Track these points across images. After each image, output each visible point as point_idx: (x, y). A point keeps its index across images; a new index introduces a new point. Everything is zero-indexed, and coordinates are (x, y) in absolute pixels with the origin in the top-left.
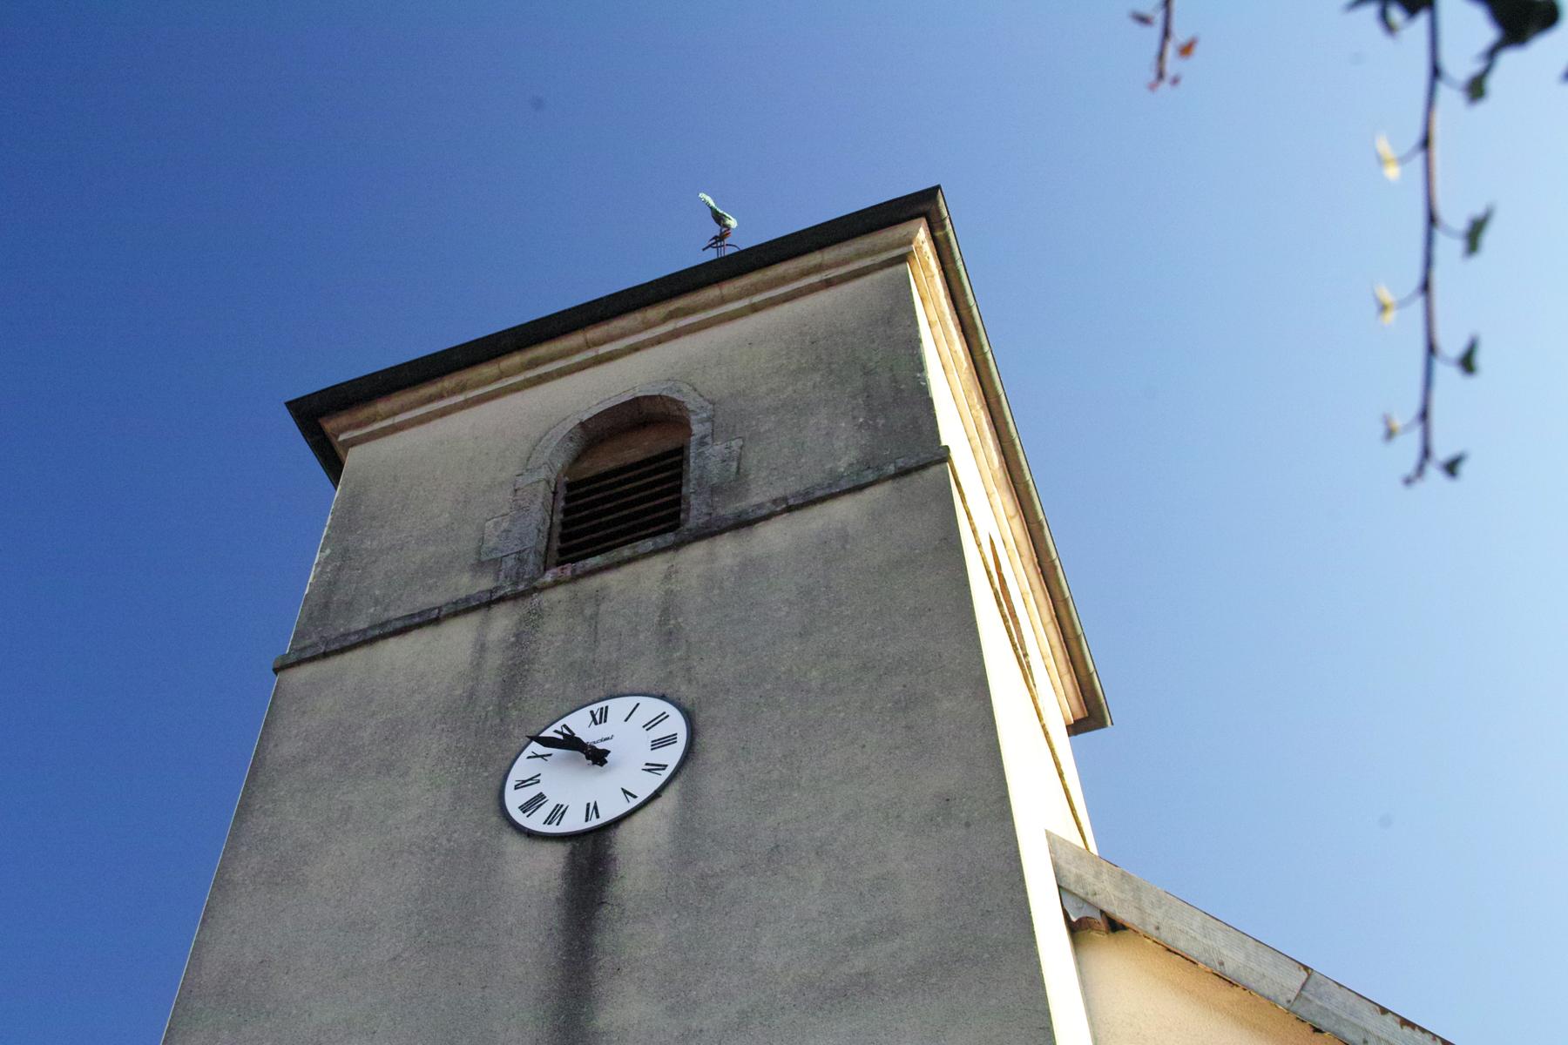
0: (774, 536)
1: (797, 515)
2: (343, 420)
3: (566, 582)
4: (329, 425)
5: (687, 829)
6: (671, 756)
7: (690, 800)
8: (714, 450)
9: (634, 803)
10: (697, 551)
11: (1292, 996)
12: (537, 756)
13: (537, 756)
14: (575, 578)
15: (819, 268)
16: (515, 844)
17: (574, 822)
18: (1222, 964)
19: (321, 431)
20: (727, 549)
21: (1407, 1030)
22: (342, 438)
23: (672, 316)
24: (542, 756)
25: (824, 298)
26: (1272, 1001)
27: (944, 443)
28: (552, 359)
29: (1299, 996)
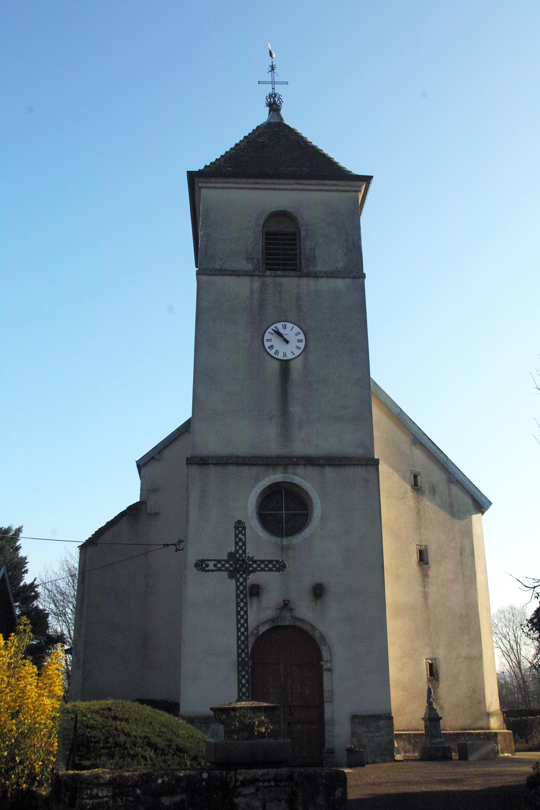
0: (324, 284)
1: (329, 278)
2: (202, 180)
3: (272, 276)
4: (197, 180)
5: (306, 366)
6: (302, 345)
7: (306, 359)
8: (517, 614)
9: (294, 356)
10: (304, 280)
11: (397, 414)
12: (270, 333)
13: (270, 333)
14: (274, 276)
15: (337, 185)
16: (268, 358)
17: (280, 356)
18: (387, 405)
19: (194, 181)
20: (312, 282)
21: (414, 424)
22: (200, 185)
23: (298, 184)
24: (272, 334)
25: (337, 194)
26: (394, 414)
27: (364, 272)
28: (262, 184)
29: (399, 414)
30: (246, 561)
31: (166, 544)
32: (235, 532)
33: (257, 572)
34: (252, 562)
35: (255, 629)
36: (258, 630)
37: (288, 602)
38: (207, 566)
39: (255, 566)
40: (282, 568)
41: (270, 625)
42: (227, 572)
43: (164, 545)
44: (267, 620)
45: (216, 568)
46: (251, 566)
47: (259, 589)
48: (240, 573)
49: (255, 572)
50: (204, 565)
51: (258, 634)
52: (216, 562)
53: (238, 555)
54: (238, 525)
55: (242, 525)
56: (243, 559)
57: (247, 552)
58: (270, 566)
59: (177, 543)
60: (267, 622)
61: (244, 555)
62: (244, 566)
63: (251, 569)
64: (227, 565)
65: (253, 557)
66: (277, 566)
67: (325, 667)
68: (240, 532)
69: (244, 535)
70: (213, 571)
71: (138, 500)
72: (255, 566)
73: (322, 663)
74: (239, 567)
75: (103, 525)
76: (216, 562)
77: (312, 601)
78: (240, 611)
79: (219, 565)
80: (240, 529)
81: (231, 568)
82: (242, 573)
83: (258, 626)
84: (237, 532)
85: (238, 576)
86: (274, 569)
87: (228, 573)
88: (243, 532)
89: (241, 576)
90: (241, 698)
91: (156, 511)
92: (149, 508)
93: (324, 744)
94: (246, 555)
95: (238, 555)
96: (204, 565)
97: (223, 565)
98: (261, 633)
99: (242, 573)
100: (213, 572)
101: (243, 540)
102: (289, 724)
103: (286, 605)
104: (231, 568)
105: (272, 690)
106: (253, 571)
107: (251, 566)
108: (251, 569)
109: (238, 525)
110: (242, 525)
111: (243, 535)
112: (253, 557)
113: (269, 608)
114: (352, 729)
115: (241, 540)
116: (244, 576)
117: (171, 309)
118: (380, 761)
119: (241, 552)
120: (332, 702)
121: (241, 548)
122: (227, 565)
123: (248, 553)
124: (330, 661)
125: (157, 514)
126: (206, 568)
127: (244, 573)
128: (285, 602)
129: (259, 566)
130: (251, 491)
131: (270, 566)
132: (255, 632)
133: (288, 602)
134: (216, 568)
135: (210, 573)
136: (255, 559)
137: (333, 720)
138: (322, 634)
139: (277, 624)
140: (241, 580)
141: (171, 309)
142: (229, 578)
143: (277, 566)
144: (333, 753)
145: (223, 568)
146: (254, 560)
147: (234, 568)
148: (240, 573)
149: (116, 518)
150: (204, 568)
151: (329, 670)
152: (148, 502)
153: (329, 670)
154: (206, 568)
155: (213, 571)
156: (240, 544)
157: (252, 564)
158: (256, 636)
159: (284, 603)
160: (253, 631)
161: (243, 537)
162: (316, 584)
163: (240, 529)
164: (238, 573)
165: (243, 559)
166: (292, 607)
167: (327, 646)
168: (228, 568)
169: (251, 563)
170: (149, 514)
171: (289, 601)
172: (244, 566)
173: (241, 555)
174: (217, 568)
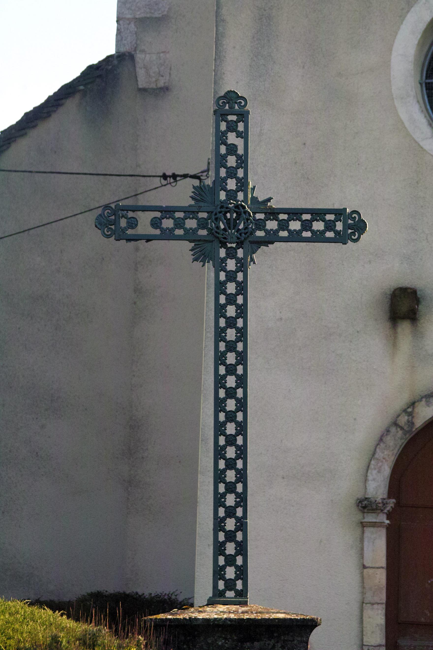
30: (246, 212)
31: (169, 173)
32: (218, 126)
33: (277, 244)
34: (265, 213)
35: (405, 411)
36: (410, 414)
38: (133, 223)
39: (272, 225)
40: (353, 234)
42: (191, 241)
43: (165, 177)
45: (158, 232)
46: (260, 225)
48: (229, 245)
49: (272, 243)
50: (123, 223)
51: (411, 423)
52: (158, 214)
53: (223, 196)
54: (227, 107)
55: (236, 107)
56: (237, 207)
57: (251, 186)
58: (318, 226)
59: (202, 172)
61: (240, 196)
62: (241, 226)
63: (260, 234)
64: (191, 224)
65: (269, 200)
66: (339, 226)
68: (232, 127)
69: (244, 135)
70: (149, 239)
71: (112, 51)
72: (272, 225)
74: (225, 230)
75: (13, 122)
76: (158, 214)
78: (224, 354)
79: (168, 223)
80: (233, 118)
81: (203, 232)
82: (234, 245)
83: (413, 404)
84: (223, 126)
85: (222, 253)
86: (330, 234)
87: (193, 244)
88: (241, 127)
89: (231, 254)
90: (222, 594)
91: (161, 84)
92: (141, 73)
94: (246, 196)
95: (223, 196)
96: (123, 223)
97: (179, 224)
98: (419, 422)
99: (234, 245)
100: (148, 241)
101: (241, 151)
104: (203, 232)
106: (266, 242)
107: (260, 225)
108: (260, 234)
109: (227, 107)
110: (236, 107)
111: (239, 135)
112: (269, 200)
115: (232, 150)
116: (240, 253)
119: (232, 184)
121: (232, 173)
122: (191, 224)
123: (253, 189)
125: (165, 89)
126: (130, 232)
127: (240, 244)
129: (283, 225)
130: (402, 17)
131: (318, 226)
132: (403, 420)
134: (158, 232)
135: (142, 244)
136: (273, 204)
140: (231, 265)
142: (196, 260)
143: (339, 226)
145: (179, 232)
146: (271, 208)
147: (210, 231)
148: (229, 245)
149: (50, 99)
150: (124, 230)
152: (139, 57)
154: (130, 232)
155: (149, 239)
156: (232, 161)
157: (264, 221)
158: (405, 433)
160: (399, 416)
161: (239, 143)
163: (233, 118)
164: (223, 245)
165: (237, 207)
168: (195, 231)
169: (260, 216)
170: (144, 90)
172: (241, 226)
173: (232, 195)
174: (162, 229)
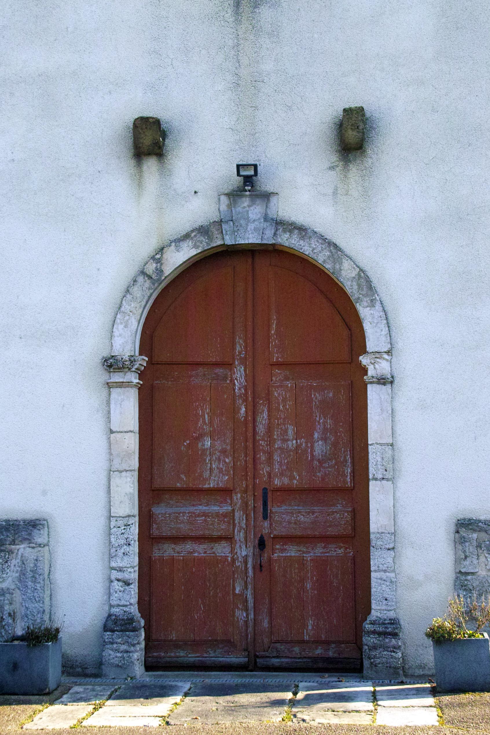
35: (153, 258)
36: (159, 261)
37: (252, 173)
41: (195, 246)
44: (189, 229)
47: (164, 134)
51: (159, 271)
60: (187, 237)
67: (371, 372)
73: (364, 360)
77: (332, 168)
83: (161, 250)
93: (368, 610)
102: (262, 544)
103: (248, 180)
105: (208, 443)
113: (195, 192)
114: (457, 561)
117: (44, 493)
118: (346, 264)
120: (392, 480)
124: (388, 352)
128: (243, 173)
132: (151, 268)
133: (252, 173)
137: (394, 534)
138: (361, 270)
139: (219, 242)
141: (44, 493)
144: (395, 635)
151: (382, 381)
153: (382, 381)
159: (238, 174)
162: (345, 110)
166: (269, 188)
167: (378, 304)
171: (255, 166)
